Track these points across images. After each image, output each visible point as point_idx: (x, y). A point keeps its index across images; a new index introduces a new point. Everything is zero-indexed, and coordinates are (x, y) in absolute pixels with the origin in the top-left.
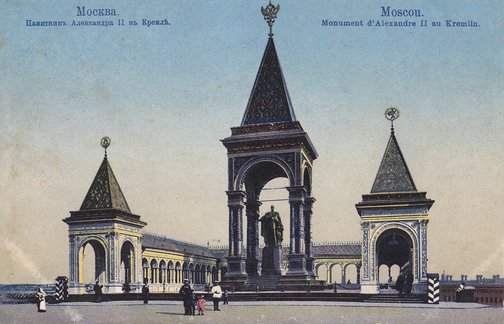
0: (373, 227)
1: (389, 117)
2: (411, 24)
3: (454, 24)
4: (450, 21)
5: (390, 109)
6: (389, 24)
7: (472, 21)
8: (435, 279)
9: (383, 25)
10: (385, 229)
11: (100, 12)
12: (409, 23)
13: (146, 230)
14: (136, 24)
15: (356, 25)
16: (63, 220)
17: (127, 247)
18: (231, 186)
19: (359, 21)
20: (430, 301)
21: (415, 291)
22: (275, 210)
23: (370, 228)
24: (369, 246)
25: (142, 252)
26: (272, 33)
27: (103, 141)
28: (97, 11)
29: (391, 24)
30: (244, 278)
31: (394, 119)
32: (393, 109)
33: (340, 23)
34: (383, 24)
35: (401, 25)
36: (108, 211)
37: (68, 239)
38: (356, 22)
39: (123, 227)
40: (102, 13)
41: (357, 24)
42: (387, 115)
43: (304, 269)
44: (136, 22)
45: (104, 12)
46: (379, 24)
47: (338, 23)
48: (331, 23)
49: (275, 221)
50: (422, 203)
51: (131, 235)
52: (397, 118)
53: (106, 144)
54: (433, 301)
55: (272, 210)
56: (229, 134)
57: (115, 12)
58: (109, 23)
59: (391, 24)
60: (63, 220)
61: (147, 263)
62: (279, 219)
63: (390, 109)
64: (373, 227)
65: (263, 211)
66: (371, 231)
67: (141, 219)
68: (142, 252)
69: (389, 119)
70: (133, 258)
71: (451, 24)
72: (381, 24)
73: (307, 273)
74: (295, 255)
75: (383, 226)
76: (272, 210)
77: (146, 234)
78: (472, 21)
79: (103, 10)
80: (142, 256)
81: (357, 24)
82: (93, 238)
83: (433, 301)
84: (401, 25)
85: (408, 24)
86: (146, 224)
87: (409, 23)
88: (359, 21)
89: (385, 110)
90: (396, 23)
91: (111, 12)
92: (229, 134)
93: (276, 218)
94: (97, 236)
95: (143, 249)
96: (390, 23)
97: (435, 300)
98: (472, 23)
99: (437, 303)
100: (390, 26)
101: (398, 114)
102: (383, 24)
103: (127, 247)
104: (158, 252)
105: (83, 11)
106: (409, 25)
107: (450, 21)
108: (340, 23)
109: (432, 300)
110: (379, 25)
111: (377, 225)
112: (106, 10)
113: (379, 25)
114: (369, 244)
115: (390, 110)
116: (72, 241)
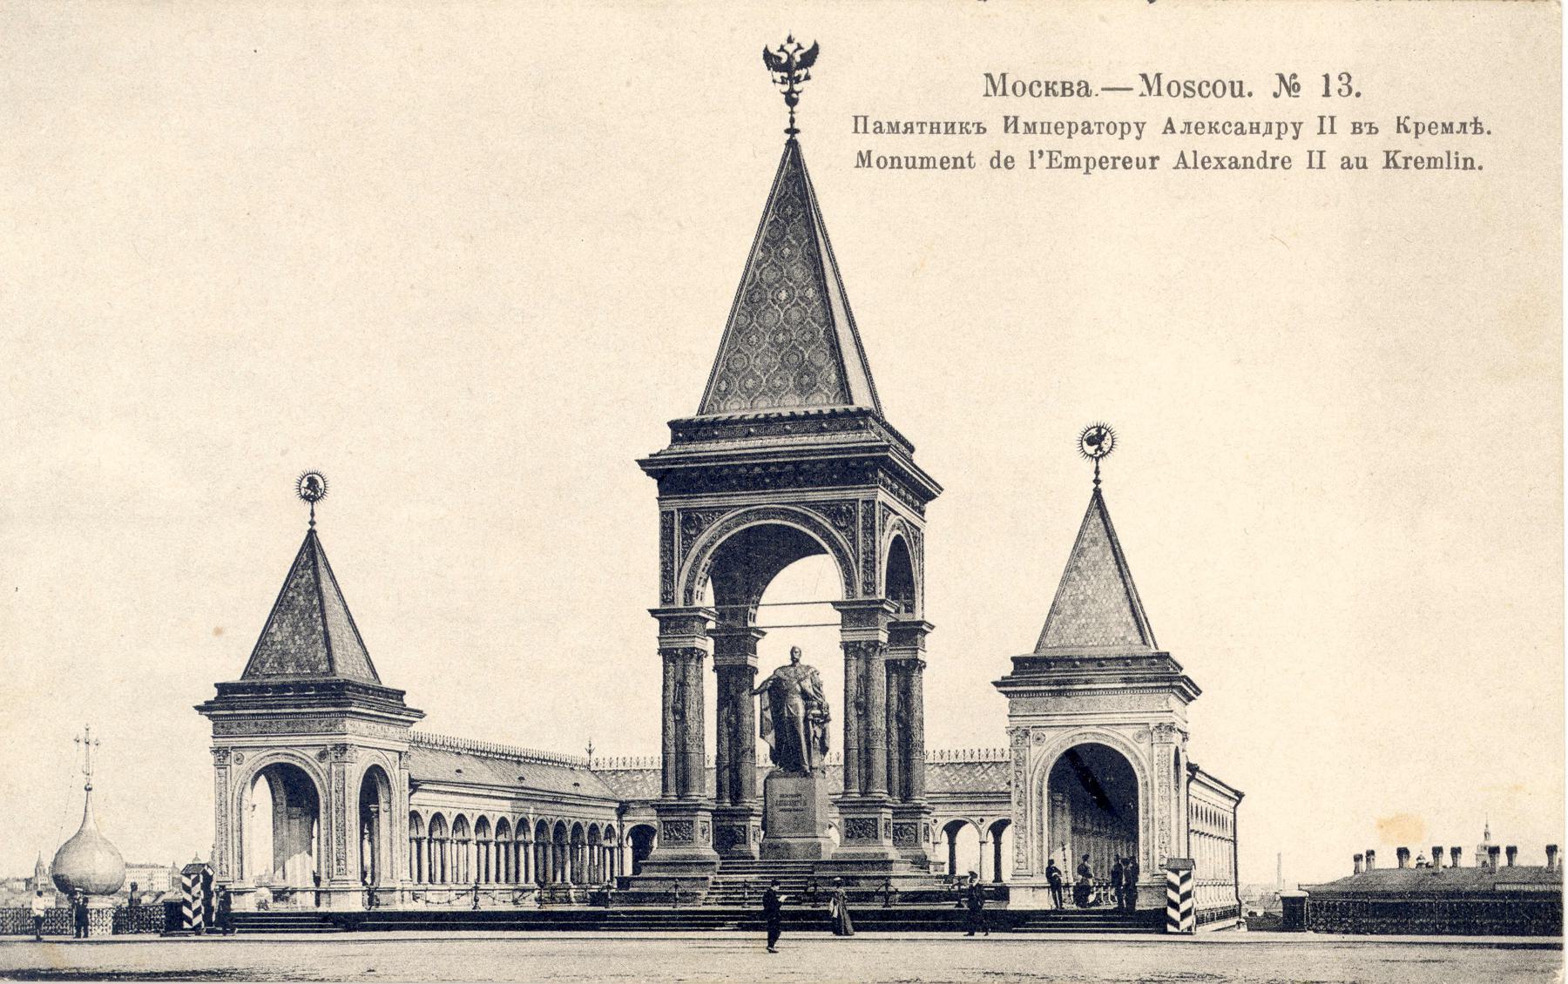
0: (239, 760)
1: (1091, 450)
2: (1278, 163)
3: (1406, 163)
4: (1396, 152)
5: (1092, 428)
6: (1214, 162)
7: (1457, 153)
8: (1182, 873)
9: (1196, 167)
10: (268, 763)
11: (1048, 89)
12: (1274, 159)
13: (419, 728)
14: (981, 130)
15: (955, 167)
16: (198, 708)
17: (374, 781)
18: (667, 595)
19: (965, 156)
20: (1170, 928)
21: (1144, 903)
22: (803, 661)
23: (233, 762)
24: (1028, 787)
25: (410, 795)
26: (796, 126)
27: (305, 483)
28: (1039, 85)
29: (1220, 162)
30: (704, 864)
31: (1101, 456)
32: (1099, 429)
33: (899, 164)
34: (1195, 163)
35: (1249, 165)
36: (321, 687)
37: (211, 758)
38: (955, 159)
39: (362, 726)
40: (1054, 91)
41: (959, 164)
42: (1085, 443)
43: (888, 842)
44: (981, 125)
45: (1058, 88)
46: (1185, 163)
47: (938, 164)
48: (882, 160)
49: (805, 695)
50: (1011, 686)
51: (382, 749)
52: (1109, 452)
53: (312, 490)
54: (1178, 928)
55: (795, 661)
56: (661, 440)
57: (1087, 87)
58: (1080, 128)
59: (1220, 162)
60: (198, 708)
61: (419, 823)
62: (818, 686)
63: (1092, 428)
64: (239, 760)
65: (767, 660)
66: (1035, 749)
67: (409, 701)
68: (410, 795)
69: (1091, 456)
70: (388, 813)
71: (1400, 161)
72: (1190, 163)
73: (893, 853)
74: (730, 810)
75: (258, 758)
76: (795, 661)
77: (459, 745)
78: (1457, 153)
79: (1055, 83)
80: (410, 804)
81: (959, 164)
82: (283, 760)
83: (1178, 928)
84: (1249, 165)
85: (1269, 164)
86: (420, 714)
87: (1274, 159)
88: (965, 156)
89: (1118, 432)
90: (1233, 160)
91: (1075, 88)
92: (661, 440)
93: (807, 684)
94: (295, 753)
95: (414, 785)
96: (1217, 159)
97: (1184, 925)
98: (1457, 159)
99: (1189, 931)
100: (1215, 168)
101: (1113, 442)
102: (1195, 163)
103: (374, 781)
104: (438, 792)
105: (1001, 85)
106: (1406, 167)
107: (1396, 152)
108: (899, 164)
109: (1176, 925)
110: (1186, 167)
111: (1049, 734)
112: (1064, 83)
113: (1186, 167)
114: (1028, 782)
115: (1094, 432)
116: (220, 765)
